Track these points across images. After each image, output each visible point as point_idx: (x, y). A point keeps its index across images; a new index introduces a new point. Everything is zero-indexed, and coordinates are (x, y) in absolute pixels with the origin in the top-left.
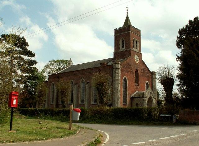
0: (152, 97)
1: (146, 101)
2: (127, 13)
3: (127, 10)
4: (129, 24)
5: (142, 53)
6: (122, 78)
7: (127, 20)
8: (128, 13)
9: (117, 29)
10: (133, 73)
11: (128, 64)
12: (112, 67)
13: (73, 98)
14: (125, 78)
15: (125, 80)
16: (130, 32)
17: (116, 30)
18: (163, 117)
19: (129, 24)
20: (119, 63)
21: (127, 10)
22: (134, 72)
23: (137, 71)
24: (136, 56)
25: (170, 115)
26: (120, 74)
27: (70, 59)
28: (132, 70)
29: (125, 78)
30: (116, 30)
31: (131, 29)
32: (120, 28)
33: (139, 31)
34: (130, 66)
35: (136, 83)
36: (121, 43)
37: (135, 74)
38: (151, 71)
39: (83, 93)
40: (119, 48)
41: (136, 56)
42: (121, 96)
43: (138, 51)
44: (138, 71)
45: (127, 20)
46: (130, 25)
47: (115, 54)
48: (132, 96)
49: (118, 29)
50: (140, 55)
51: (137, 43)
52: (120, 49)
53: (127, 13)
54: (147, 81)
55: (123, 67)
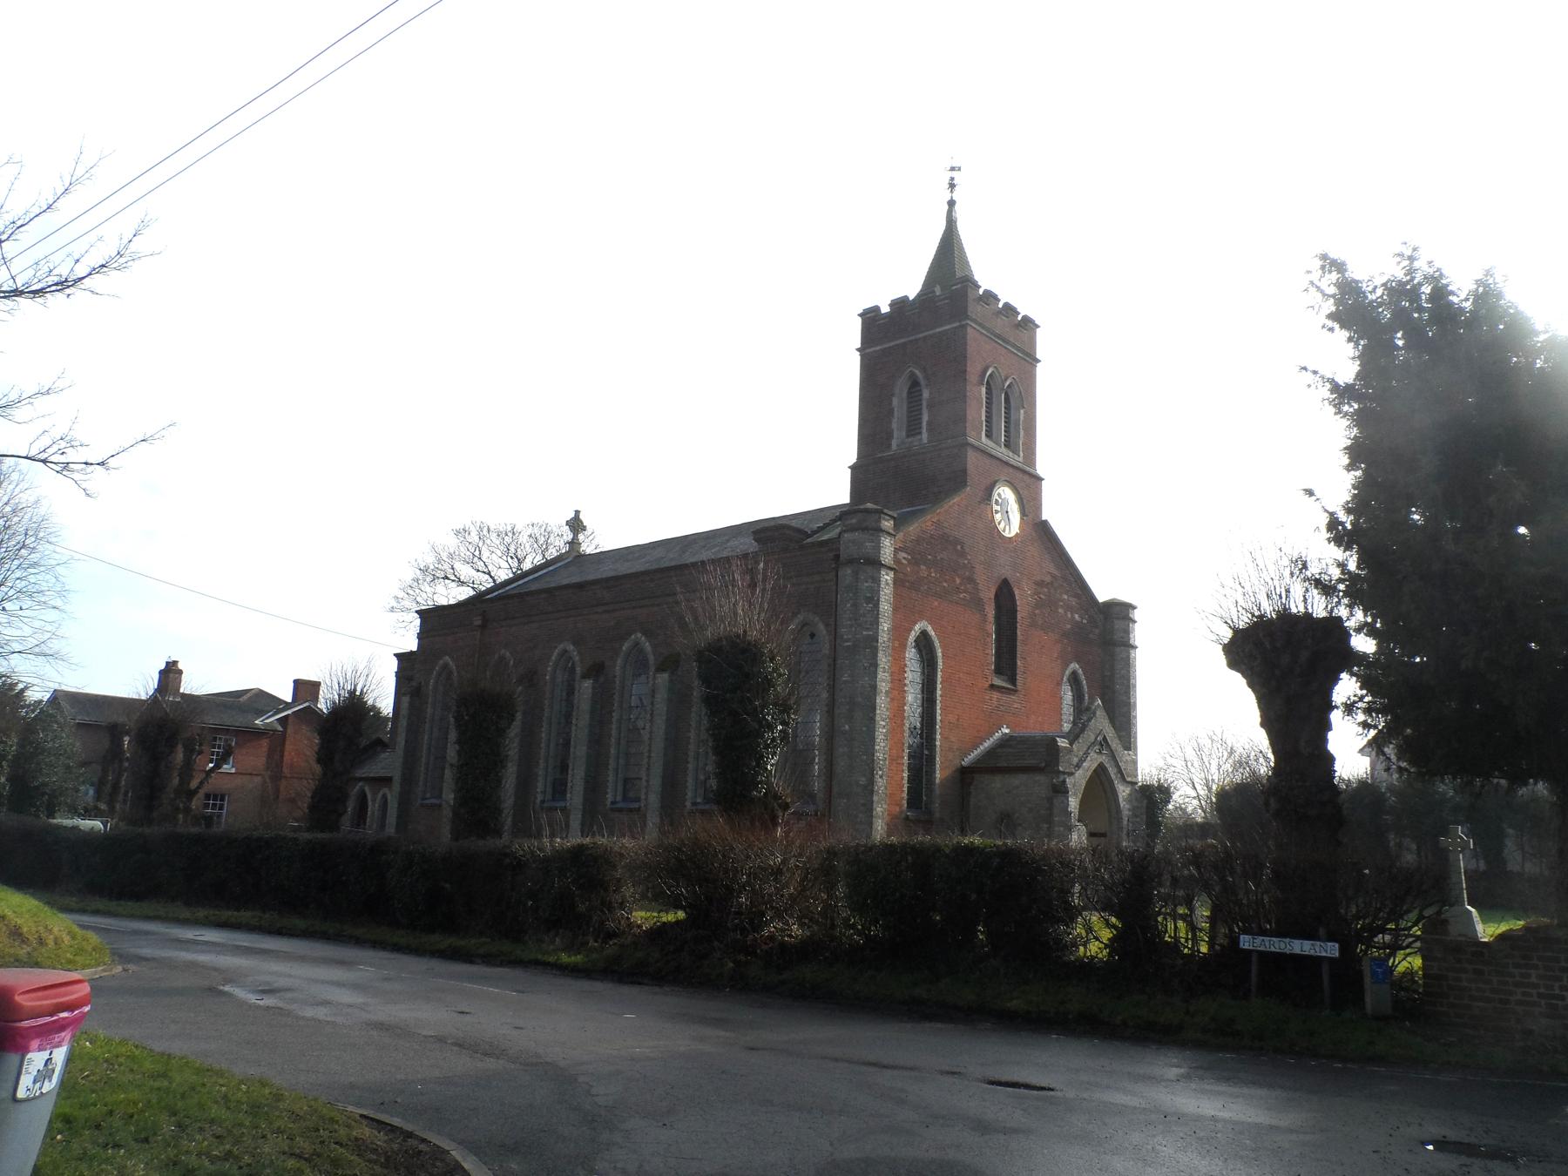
0: (1112, 771)
1: (1073, 803)
2: (951, 203)
3: (952, 186)
4: (959, 274)
5: (1040, 470)
6: (899, 632)
7: (949, 249)
8: (957, 207)
9: (876, 309)
10: (978, 603)
11: (946, 540)
12: (837, 557)
13: (256, 953)
14: (924, 633)
15: (924, 643)
16: (964, 327)
17: (871, 319)
18: (1264, 956)
19: (959, 274)
20: (887, 524)
21: (952, 186)
22: (988, 594)
23: (1005, 595)
24: (1005, 493)
25: (1331, 950)
26: (885, 607)
27: (577, 512)
28: (971, 580)
29: (924, 633)
30: (871, 319)
31: (975, 310)
32: (900, 305)
33: (1028, 325)
34: (963, 554)
35: (999, 671)
36: (898, 403)
37: (991, 612)
38: (1102, 596)
39: (341, 1122)
40: (890, 436)
41: (1005, 493)
42: (895, 760)
43: (1017, 460)
44: (1012, 596)
45: (949, 249)
46: (969, 282)
47: (861, 474)
48: (967, 761)
49: (885, 309)
50: (1029, 487)
51: (1008, 408)
52: (894, 443)
53: (951, 203)
54: (1074, 666)
55: (915, 562)
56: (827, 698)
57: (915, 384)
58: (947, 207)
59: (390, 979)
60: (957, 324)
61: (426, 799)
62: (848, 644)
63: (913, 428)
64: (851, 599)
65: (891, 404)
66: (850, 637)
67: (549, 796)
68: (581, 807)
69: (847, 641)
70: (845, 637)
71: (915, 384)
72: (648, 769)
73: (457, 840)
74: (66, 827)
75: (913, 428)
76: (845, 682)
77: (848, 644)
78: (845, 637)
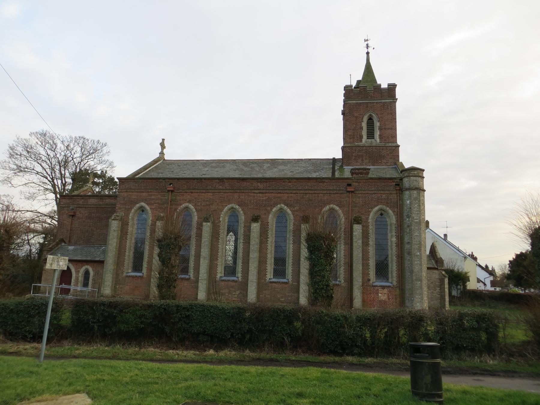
53: (368, 53)
56: (396, 241)
57: (370, 119)
58: (366, 55)
59: (69, 373)
60: (392, 101)
61: (129, 273)
62: (417, 221)
63: (371, 135)
64: (417, 203)
65: (361, 125)
66: (418, 218)
67: (223, 275)
68: (300, 284)
69: (416, 219)
70: (415, 218)
71: (370, 119)
72: (391, 272)
73: (61, 284)
74: (269, 366)
75: (371, 135)
76: (416, 236)
77: (417, 221)
78: (415, 218)
